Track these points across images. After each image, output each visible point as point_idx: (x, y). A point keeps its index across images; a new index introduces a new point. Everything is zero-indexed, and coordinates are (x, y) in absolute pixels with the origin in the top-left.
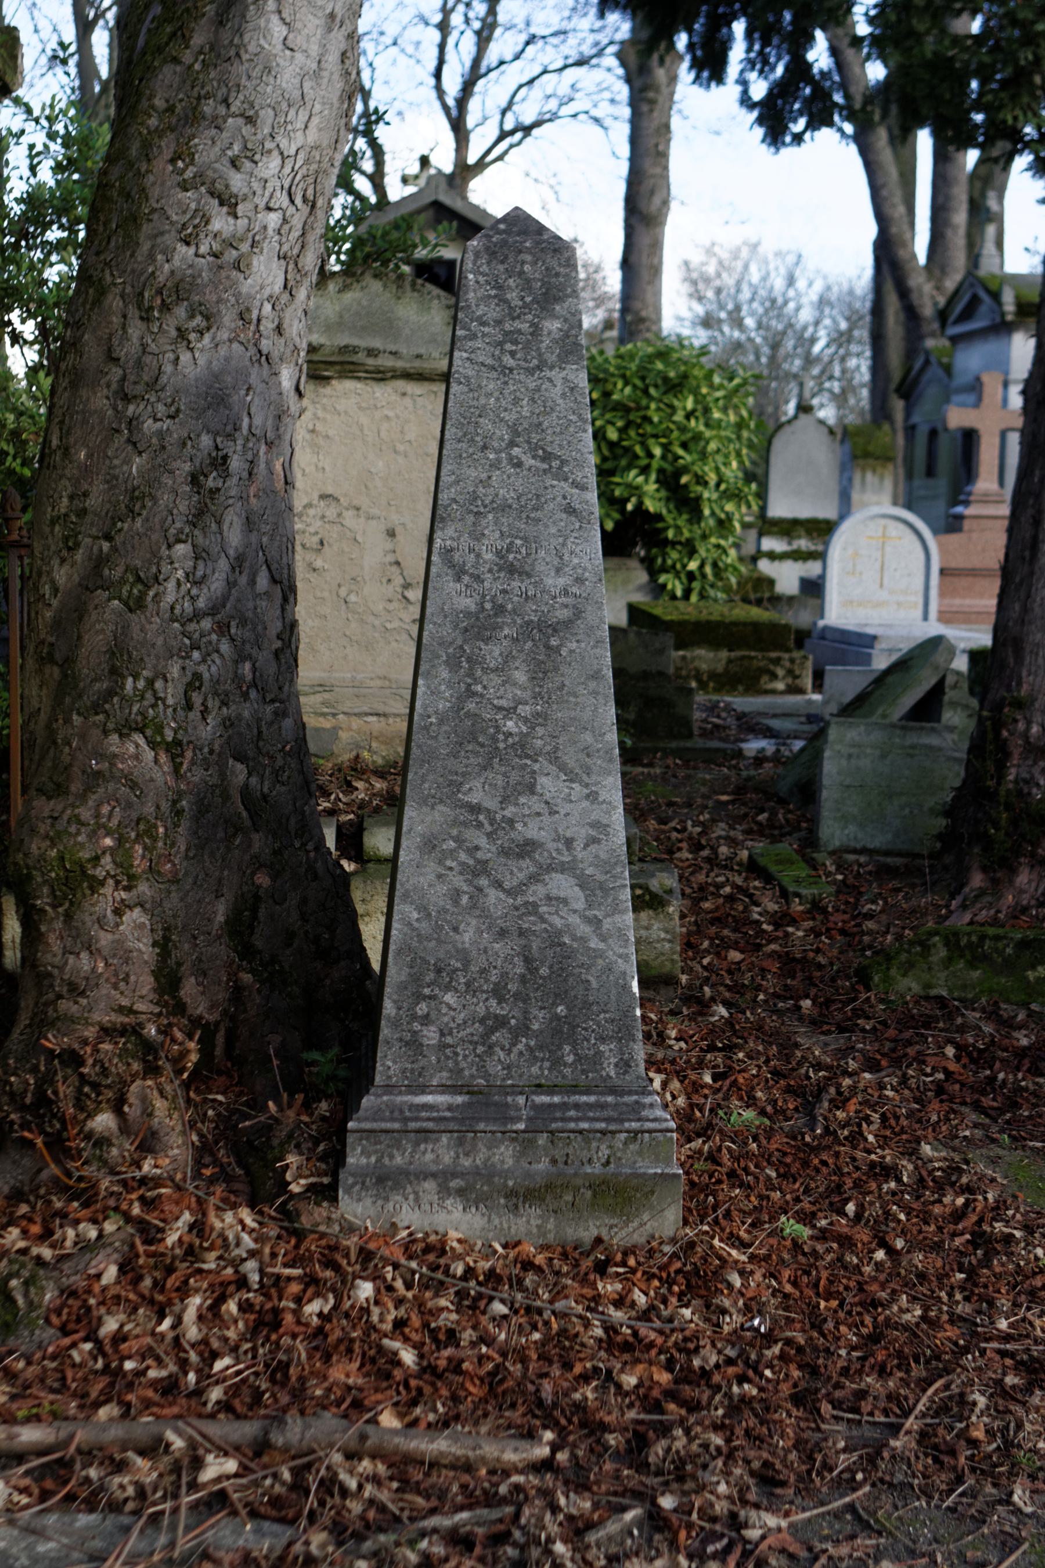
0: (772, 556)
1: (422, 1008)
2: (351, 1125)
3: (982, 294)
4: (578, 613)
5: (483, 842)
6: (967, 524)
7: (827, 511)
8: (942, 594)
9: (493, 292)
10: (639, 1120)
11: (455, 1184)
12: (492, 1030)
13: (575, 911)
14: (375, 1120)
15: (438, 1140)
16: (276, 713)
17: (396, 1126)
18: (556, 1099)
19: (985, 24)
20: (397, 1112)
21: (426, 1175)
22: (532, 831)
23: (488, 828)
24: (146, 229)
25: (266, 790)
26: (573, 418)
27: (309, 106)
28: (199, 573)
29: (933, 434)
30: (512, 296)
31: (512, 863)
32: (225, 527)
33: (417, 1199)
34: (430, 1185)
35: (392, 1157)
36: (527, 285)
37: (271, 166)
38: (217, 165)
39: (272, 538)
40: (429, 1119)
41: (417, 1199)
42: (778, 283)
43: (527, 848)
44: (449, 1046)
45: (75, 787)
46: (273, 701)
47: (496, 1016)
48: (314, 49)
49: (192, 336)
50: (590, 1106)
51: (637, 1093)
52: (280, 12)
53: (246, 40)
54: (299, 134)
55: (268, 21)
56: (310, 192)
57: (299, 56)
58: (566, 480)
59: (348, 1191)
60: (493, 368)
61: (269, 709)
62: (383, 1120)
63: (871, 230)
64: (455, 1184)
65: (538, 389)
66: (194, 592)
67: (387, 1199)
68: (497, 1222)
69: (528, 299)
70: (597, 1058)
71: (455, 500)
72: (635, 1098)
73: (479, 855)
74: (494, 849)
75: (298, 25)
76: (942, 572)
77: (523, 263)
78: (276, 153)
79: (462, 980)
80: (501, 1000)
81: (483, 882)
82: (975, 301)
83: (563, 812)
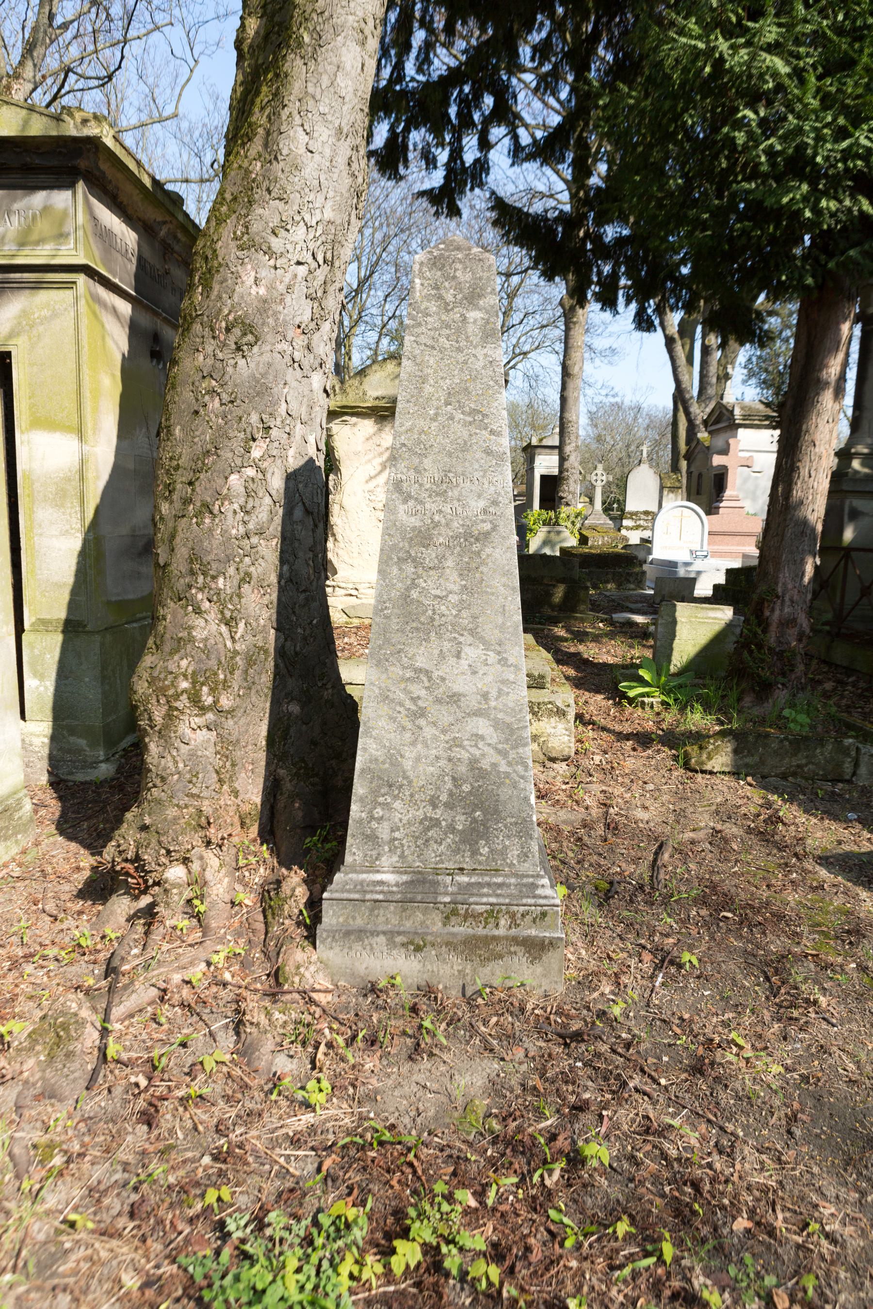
0: (628, 528)
1: (379, 812)
2: (325, 895)
3: (724, 411)
4: (495, 528)
5: (423, 693)
6: (721, 510)
7: (654, 508)
8: (709, 544)
9: (433, 292)
10: (534, 897)
11: (399, 939)
12: (428, 829)
13: (489, 745)
14: (343, 892)
15: (387, 908)
16: (307, 599)
17: (356, 896)
18: (473, 880)
19: (721, 303)
20: (362, 888)
21: (375, 933)
22: (458, 686)
23: (427, 684)
24: (217, 277)
25: (298, 649)
26: (491, 383)
27: (324, 190)
28: (249, 507)
29: (700, 476)
30: (449, 298)
31: (444, 708)
32: (268, 476)
33: (372, 949)
34: (382, 939)
35: (354, 918)
36: (458, 288)
37: (299, 233)
38: (264, 234)
39: (306, 486)
40: (381, 892)
41: (372, 949)
42: (630, 421)
43: (454, 698)
44: (396, 839)
45: (167, 648)
46: (304, 591)
47: (431, 819)
48: (328, 152)
49: (245, 348)
50: (500, 886)
51: (533, 876)
52: (302, 125)
53: (281, 146)
54: (318, 211)
55: (295, 132)
56: (329, 256)
57: (316, 156)
58: (485, 429)
59: (322, 942)
60: (433, 348)
61: (302, 596)
62: (349, 891)
63: (672, 386)
64: (399, 939)
65: (465, 362)
66: (246, 518)
67: (350, 948)
68: (429, 967)
69: (459, 297)
70: (503, 852)
71: (404, 445)
72: (531, 880)
73: (420, 703)
74: (430, 699)
75: (316, 135)
76: (710, 533)
77: (456, 270)
78: (302, 223)
79: (407, 793)
80: (435, 807)
81: (422, 722)
82: (721, 415)
83: (481, 672)
